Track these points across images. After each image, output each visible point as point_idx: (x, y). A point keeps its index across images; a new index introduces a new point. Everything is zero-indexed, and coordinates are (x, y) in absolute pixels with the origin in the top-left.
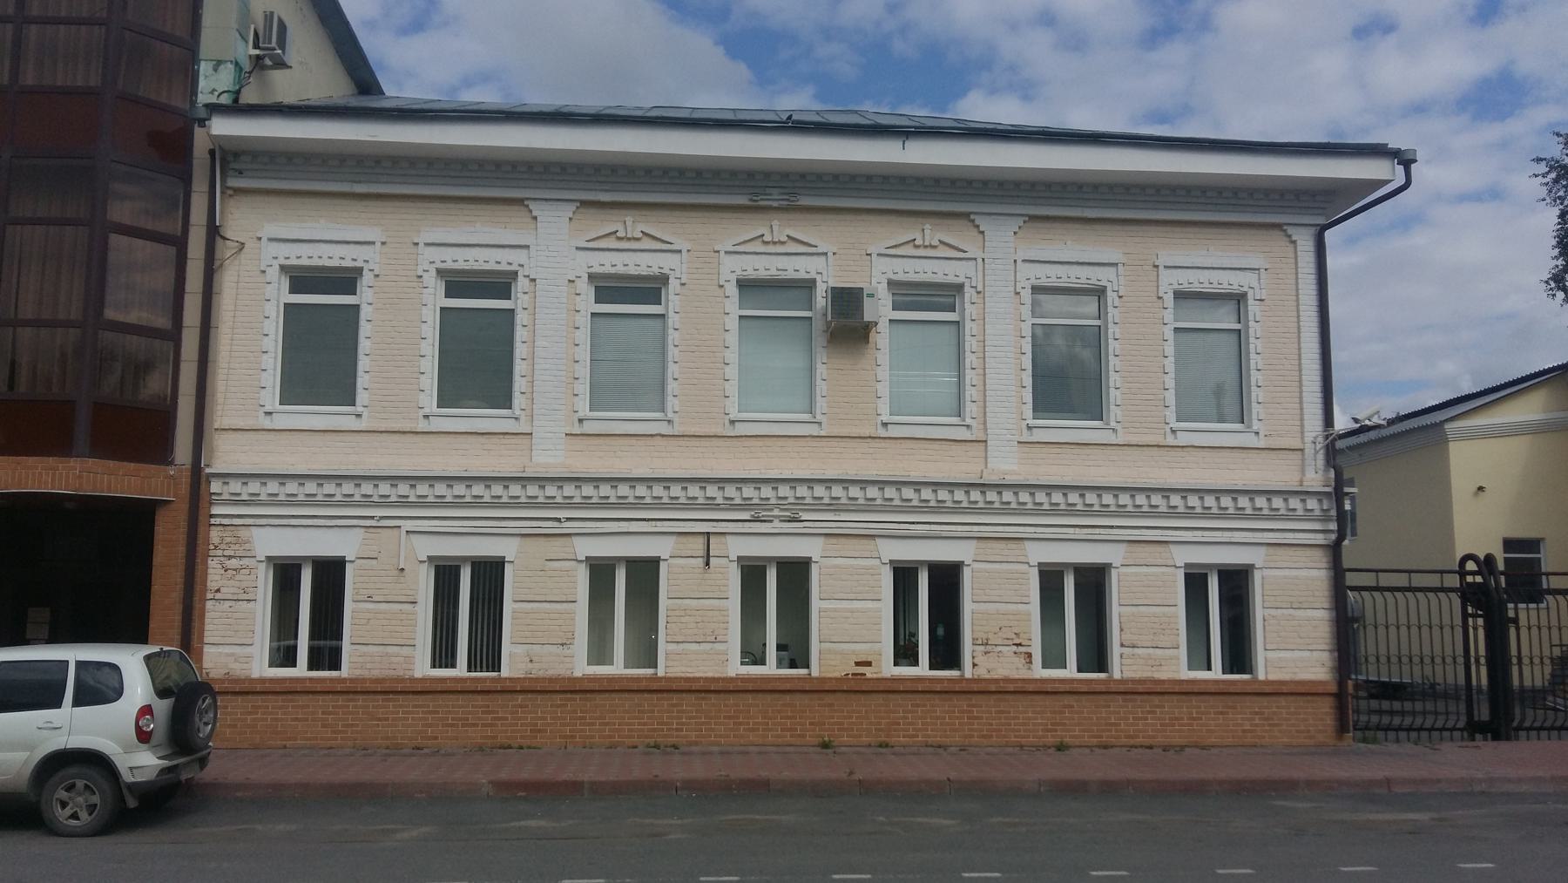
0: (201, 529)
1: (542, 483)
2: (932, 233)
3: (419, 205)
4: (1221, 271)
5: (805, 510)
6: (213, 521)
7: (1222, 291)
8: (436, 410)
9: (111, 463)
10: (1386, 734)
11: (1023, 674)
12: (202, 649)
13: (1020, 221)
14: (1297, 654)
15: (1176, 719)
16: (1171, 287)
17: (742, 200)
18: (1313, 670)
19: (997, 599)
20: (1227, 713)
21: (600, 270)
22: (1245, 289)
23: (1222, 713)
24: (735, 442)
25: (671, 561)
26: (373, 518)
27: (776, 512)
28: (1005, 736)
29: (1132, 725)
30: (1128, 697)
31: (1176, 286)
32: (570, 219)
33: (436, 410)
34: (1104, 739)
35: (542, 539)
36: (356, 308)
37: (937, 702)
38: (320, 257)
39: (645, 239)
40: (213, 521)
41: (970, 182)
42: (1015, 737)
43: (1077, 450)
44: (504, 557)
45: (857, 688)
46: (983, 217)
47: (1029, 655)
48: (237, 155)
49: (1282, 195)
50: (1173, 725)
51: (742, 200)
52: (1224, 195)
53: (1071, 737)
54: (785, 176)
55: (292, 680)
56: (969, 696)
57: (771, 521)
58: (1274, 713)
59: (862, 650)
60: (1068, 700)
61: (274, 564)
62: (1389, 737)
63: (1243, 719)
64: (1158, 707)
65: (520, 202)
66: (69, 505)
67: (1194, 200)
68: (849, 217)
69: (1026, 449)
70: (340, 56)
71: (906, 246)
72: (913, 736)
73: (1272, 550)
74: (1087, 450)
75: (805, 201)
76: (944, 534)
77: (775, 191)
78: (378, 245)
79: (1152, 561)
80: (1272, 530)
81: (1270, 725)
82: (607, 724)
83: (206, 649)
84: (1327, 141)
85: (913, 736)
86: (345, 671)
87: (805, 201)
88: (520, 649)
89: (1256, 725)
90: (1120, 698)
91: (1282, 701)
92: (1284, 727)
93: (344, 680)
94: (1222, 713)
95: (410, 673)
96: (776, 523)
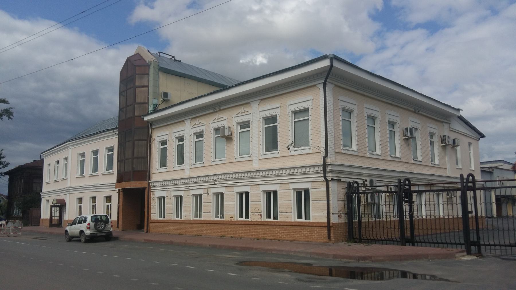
0: (150, 192)
1: (265, 171)
2: (241, 110)
3: (293, 93)
4: (302, 103)
5: (222, 181)
6: (151, 191)
7: (303, 108)
8: (177, 166)
9: (136, 182)
10: (506, 248)
11: (260, 220)
12: (151, 214)
13: (259, 101)
14: (320, 214)
15: (290, 233)
16: (261, 117)
17: (212, 111)
18: (323, 219)
19: (255, 201)
20: (302, 231)
21: (196, 132)
22: (308, 107)
23: (301, 231)
24: (213, 166)
25: (280, 191)
26: (166, 188)
27: (218, 182)
28: (255, 236)
29: (280, 234)
30: (280, 226)
31: (292, 110)
32: (259, 105)
33: (177, 166)
34: (275, 238)
35: (187, 191)
36: (277, 125)
37: (243, 227)
38: (300, 107)
39: (221, 118)
40: (151, 191)
41: (248, 95)
42: (258, 236)
43: (271, 160)
44: (308, 188)
45: (231, 223)
46: (319, 85)
47: (261, 215)
48: (152, 122)
49: (299, 81)
50: (289, 234)
51: (212, 111)
52: (289, 84)
53: (268, 237)
54: (218, 103)
55: (269, 222)
56: (249, 225)
57: (217, 184)
58: (313, 232)
59: (231, 214)
60: (268, 227)
61: (296, 192)
62: (427, 245)
63: (305, 233)
64: (286, 229)
65: (315, 85)
66: (141, 189)
67: (320, 77)
68: (158, 129)
69: (261, 161)
70: (205, 83)
71: (239, 114)
72: (239, 235)
73: (313, 183)
74: (273, 159)
75: (222, 108)
76: (244, 185)
77: (217, 107)
78: (279, 108)
79: (285, 189)
80: (312, 177)
81: (312, 235)
82: (194, 230)
83: (151, 214)
84: (310, 60)
85: (239, 235)
86: (279, 220)
87: (222, 108)
88: (184, 214)
89: (309, 235)
90: (278, 226)
91: (315, 228)
92: (316, 236)
93: (183, 220)
94: (301, 231)
95: (396, 224)
96: (218, 185)
